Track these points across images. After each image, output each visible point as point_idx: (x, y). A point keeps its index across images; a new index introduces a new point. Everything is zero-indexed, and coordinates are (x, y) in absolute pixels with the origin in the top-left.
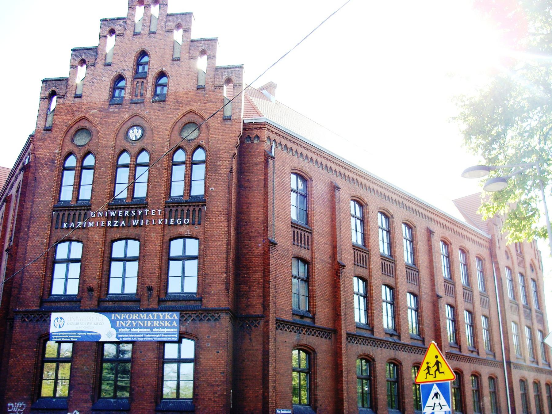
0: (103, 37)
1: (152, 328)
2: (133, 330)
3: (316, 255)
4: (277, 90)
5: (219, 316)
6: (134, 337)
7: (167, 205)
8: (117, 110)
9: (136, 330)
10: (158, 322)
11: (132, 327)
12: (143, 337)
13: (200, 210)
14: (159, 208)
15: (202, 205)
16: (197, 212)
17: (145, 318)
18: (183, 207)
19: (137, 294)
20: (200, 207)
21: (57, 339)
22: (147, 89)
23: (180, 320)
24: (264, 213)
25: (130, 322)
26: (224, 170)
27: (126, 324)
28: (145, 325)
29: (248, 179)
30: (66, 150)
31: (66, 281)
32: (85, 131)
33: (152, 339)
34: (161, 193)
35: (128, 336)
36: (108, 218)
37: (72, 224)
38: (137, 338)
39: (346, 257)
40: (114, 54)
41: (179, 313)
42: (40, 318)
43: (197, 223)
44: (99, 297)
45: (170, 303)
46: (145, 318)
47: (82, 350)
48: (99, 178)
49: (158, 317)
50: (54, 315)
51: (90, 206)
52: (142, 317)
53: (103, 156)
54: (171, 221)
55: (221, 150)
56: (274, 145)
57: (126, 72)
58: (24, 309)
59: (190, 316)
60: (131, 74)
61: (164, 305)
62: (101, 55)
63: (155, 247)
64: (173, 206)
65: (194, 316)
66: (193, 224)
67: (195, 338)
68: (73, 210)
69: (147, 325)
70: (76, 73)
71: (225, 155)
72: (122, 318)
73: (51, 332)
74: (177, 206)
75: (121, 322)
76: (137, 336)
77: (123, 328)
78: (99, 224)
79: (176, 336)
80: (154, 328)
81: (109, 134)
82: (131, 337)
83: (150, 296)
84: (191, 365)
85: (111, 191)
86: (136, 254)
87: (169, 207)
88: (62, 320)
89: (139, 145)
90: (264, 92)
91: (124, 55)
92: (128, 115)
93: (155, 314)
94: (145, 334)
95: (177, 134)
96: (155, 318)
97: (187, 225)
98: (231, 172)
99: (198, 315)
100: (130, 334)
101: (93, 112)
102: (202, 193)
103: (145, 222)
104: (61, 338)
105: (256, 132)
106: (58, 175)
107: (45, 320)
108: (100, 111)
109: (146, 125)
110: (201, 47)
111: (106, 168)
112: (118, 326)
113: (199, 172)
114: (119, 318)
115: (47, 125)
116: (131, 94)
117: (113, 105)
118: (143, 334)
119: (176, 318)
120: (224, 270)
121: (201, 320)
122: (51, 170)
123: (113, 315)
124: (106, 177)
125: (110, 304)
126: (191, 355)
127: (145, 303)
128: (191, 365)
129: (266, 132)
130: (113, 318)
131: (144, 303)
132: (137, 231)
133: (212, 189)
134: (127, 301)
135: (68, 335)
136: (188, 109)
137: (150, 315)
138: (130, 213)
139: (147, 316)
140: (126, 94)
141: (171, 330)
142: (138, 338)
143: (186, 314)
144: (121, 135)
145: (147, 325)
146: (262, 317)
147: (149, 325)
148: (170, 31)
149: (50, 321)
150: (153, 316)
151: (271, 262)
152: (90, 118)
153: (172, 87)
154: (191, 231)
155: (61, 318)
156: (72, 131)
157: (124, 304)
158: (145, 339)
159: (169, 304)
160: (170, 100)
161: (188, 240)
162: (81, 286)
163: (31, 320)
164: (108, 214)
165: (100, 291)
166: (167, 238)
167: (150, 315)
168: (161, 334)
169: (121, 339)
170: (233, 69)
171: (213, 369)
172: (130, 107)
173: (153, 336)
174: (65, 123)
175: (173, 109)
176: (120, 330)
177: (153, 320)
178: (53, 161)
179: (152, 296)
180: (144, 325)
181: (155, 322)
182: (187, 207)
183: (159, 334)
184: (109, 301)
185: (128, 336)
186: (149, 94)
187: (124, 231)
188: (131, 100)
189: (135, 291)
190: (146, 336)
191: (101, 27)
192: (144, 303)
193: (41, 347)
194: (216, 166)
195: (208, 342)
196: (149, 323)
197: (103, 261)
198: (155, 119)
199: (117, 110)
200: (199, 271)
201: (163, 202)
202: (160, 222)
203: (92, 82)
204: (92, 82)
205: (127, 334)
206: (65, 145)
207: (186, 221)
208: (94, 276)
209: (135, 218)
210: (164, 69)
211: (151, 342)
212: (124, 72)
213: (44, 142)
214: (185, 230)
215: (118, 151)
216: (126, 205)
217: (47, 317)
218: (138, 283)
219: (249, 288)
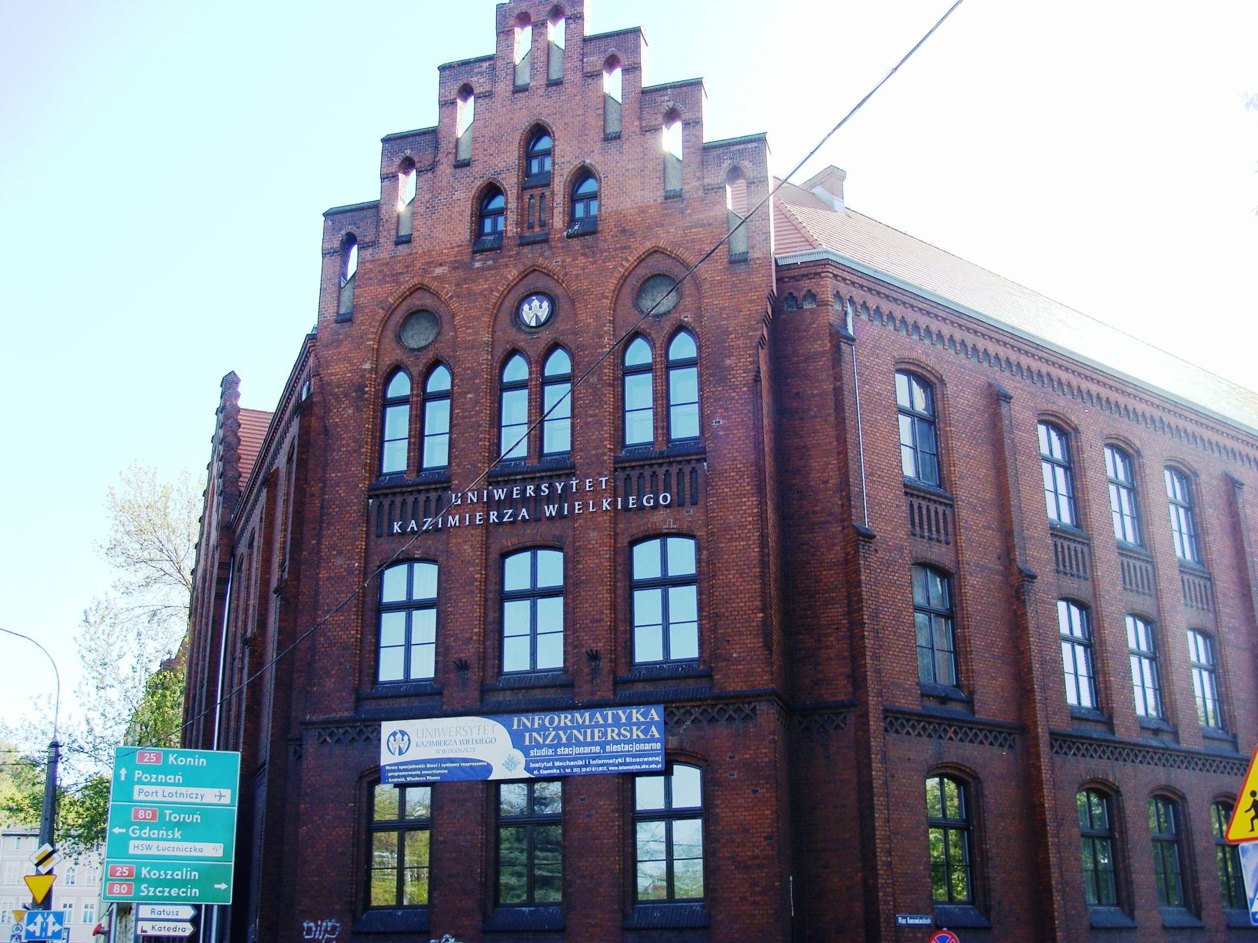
1: (603, 745)
3: (967, 555)
11: (560, 745)
27: (545, 740)
30: (387, 361)
31: (408, 649)
36: (491, 504)
39: (1037, 556)
50: (387, 727)
65: (696, 712)
83: (595, 672)
98: (757, 379)
101: (438, 271)
105: (806, 284)
117: (481, 251)
121: (712, 720)
122: (358, 409)
129: (829, 283)
132: (556, 529)
133: (718, 422)
136: (649, 245)
141: (648, 746)
146: (852, 704)
150: (605, 718)
152: (434, 286)
155: (403, 733)
164: (490, 496)
178: (360, 389)
186: (558, 221)
202: (605, 505)
210: (588, 161)
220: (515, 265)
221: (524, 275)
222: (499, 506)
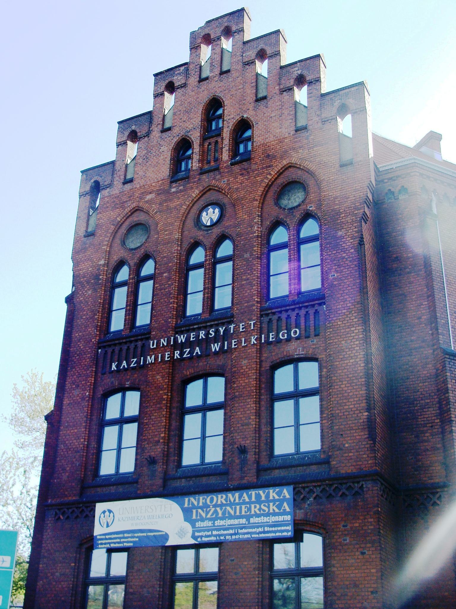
0: (158, 95)
1: (248, 518)
2: (218, 523)
4: (443, 144)
5: (362, 487)
6: (219, 535)
7: (264, 313)
8: (181, 188)
9: (222, 523)
10: (258, 506)
12: (235, 534)
13: (316, 312)
14: (251, 320)
15: (320, 304)
16: (312, 317)
17: (237, 501)
18: (289, 313)
19: (223, 462)
20: (316, 307)
21: (108, 546)
22: (222, 148)
23: (294, 500)
24: (429, 307)
25: (213, 509)
26: (349, 243)
27: (207, 513)
28: (238, 514)
29: (397, 257)
30: (115, 258)
32: (140, 227)
33: (249, 536)
34: (253, 295)
35: (210, 533)
36: (176, 346)
37: (124, 363)
38: (225, 535)
40: (174, 114)
41: (291, 488)
42: (81, 512)
43: (312, 333)
44: (166, 473)
45: (277, 471)
46: (237, 501)
47: (140, 562)
48: (161, 290)
49: (258, 496)
50: (100, 507)
51: (150, 333)
52: (232, 500)
53: (165, 257)
54: (271, 337)
55: (342, 213)
56: (434, 198)
57: (191, 133)
58: (58, 501)
59: (311, 491)
60: (199, 134)
61: (266, 477)
62: (157, 120)
63: (249, 381)
64: (274, 313)
66: (308, 337)
67: (321, 531)
68: (126, 343)
69: (241, 512)
70: (125, 151)
71: (349, 219)
72: (201, 504)
73: (95, 534)
74: (280, 312)
75: (200, 511)
76: (225, 532)
77: (202, 520)
78: (163, 357)
79: (289, 528)
80: (252, 516)
81: (172, 224)
82: (215, 536)
84: (320, 581)
85: (178, 306)
86: (221, 398)
87: (267, 315)
88: (112, 514)
89: (217, 231)
90: (423, 149)
91: (187, 112)
92: (197, 192)
93: (253, 493)
94: (238, 528)
95: (273, 203)
96: (253, 499)
97: (297, 338)
99: (324, 489)
100: (214, 530)
101: (149, 197)
102: (319, 286)
103: (230, 344)
104: (109, 543)
106: (105, 295)
107: (87, 516)
108: (158, 194)
109: (226, 201)
110: (296, 72)
111: (169, 272)
112: (194, 517)
113: (311, 254)
114: (196, 503)
115: (90, 230)
116: (201, 161)
117: (175, 181)
118: (235, 528)
119: (288, 496)
120: (364, 405)
122: (95, 290)
123: (187, 499)
124: (170, 286)
125: (183, 483)
126: (318, 562)
127: (237, 474)
128: (320, 581)
130: (186, 505)
131: (235, 476)
134: (209, 475)
135: (120, 538)
137: (245, 495)
138: (208, 334)
139: (240, 497)
140: (195, 164)
141: (281, 518)
142: (228, 536)
143: (304, 488)
144: (190, 223)
145: (241, 512)
147: (243, 513)
148: (251, 63)
149: (94, 516)
150: (250, 497)
151: (450, 386)
152: (146, 206)
153: (258, 139)
154: (304, 348)
155: (110, 511)
156: (123, 230)
157: (204, 480)
158: (237, 537)
159: (277, 473)
160: (258, 157)
161: (301, 365)
162: (139, 457)
163: (68, 518)
164: (176, 340)
165: (167, 463)
166: (266, 365)
167: (245, 495)
168: (264, 526)
169: (199, 539)
170: (347, 90)
171: (356, 586)
172: (199, 179)
173: (250, 530)
174: (113, 221)
175: (263, 168)
176: (198, 524)
177: (250, 503)
179: (250, 465)
180: (235, 512)
181: (253, 506)
182: (296, 311)
183: (261, 526)
184: (180, 478)
185: (210, 533)
186: (225, 156)
187: (201, 364)
188: (201, 169)
189: (220, 459)
190: (240, 531)
191: (156, 84)
192: (235, 476)
193: (82, 561)
194: (336, 238)
195: (346, 535)
196: (244, 510)
197: (171, 414)
198: (237, 189)
199: (181, 188)
200: (322, 412)
201: (256, 308)
202: (253, 341)
203: (146, 158)
204: (146, 158)
205: (208, 531)
206: (113, 252)
207: (295, 332)
208: (157, 439)
209: (215, 340)
210: (245, 116)
211: (247, 541)
212: (189, 134)
213: (85, 252)
214: (295, 349)
215: (186, 246)
216: (201, 323)
217: (90, 511)
218: (224, 444)
219: (417, 437)
220: (197, 187)
221: (203, 193)
222: (181, 347)
